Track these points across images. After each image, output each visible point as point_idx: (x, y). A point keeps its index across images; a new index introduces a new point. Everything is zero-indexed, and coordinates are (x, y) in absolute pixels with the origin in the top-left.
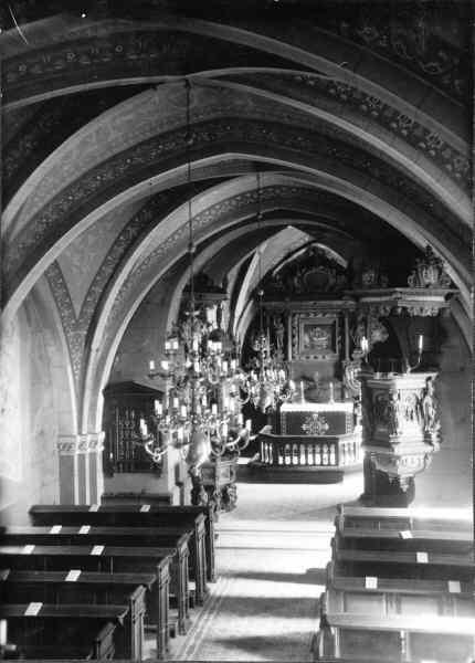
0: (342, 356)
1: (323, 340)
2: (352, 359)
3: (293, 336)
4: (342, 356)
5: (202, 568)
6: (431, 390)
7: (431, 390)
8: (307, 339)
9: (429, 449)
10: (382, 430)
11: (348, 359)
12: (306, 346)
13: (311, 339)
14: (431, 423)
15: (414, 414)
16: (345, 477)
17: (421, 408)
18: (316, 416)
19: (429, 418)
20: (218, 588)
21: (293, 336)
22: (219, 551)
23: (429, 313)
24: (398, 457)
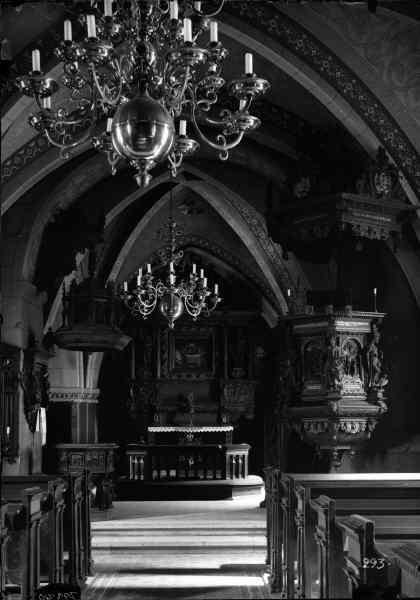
0: (220, 374)
1: (196, 357)
2: (230, 377)
3: (163, 352)
4: (220, 374)
5: (320, 398)
6: (378, 336)
7: (378, 336)
8: (179, 357)
9: (374, 409)
10: (313, 387)
11: (227, 377)
12: (176, 364)
13: (182, 355)
14: (376, 377)
15: (355, 366)
16: (258, 505)
17: (365, 357)
18: (191, 437)
19: (375, 371)
20: (304, 399)
21: (163, 352)
22: (96, 552)
23: (378, 237)
24: (112, 507)
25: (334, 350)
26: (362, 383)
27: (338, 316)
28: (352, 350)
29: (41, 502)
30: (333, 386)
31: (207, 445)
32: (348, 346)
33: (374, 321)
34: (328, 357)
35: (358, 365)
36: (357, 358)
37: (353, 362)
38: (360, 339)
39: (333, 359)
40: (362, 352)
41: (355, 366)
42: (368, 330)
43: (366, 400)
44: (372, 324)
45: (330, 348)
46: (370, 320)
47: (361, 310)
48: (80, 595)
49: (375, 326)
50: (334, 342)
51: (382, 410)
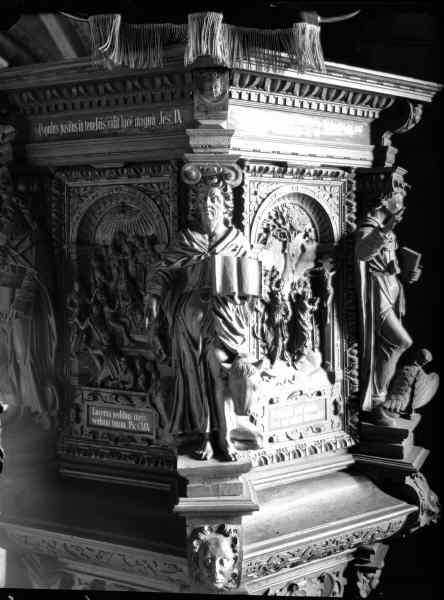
15: (306, 317)
19: (387, 337)
25: (223, 252)
26: (334, 392)
27: (250, 80)
28: (298, 240)
29: (247, 449)
30: (217, 440)
31: (415, 253)
32: (280, 229)
33: (389, 117)
34: (197, 292)
35: (320, 317)
36: (316, 279)
37: (298, 303)
38: (330, 199)
39: (211, 301)
40: (338, 257)
41: (306, 317)
42: (362, 157)
43: (351, 471)
44: (376, 131)
45: (200, 240)
46: (374, 113)
47: (331, 61)
48: (87, 211)
49: (387, 141)
50: (218, 212)
51: (423, 520)
